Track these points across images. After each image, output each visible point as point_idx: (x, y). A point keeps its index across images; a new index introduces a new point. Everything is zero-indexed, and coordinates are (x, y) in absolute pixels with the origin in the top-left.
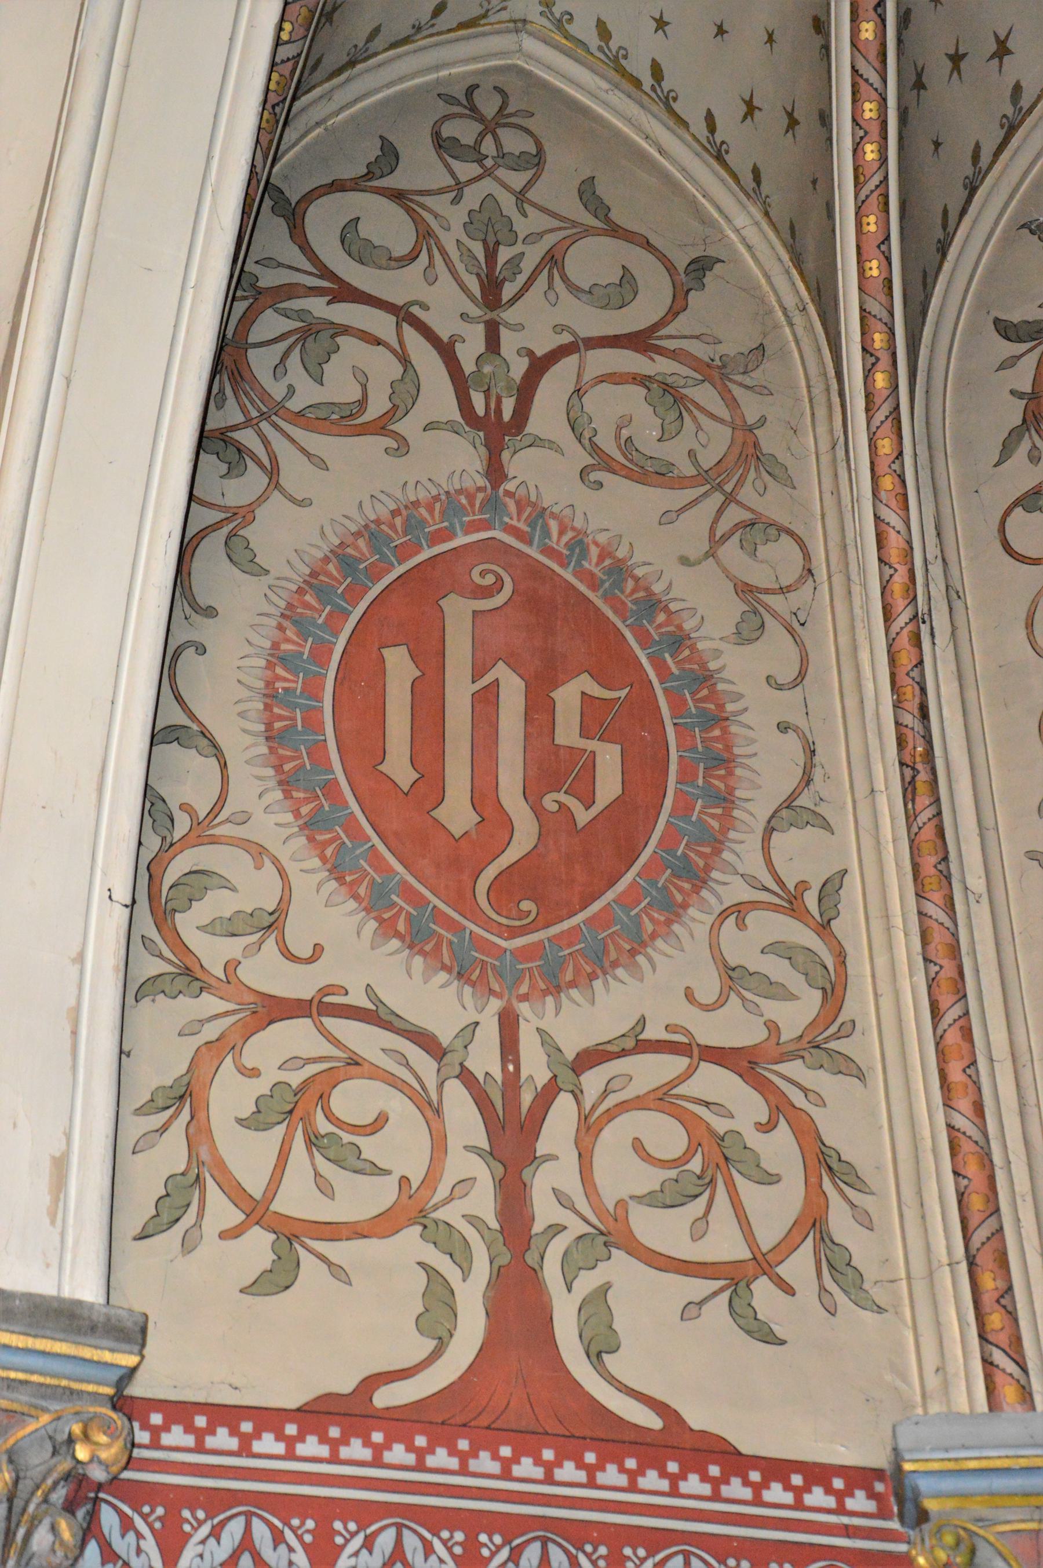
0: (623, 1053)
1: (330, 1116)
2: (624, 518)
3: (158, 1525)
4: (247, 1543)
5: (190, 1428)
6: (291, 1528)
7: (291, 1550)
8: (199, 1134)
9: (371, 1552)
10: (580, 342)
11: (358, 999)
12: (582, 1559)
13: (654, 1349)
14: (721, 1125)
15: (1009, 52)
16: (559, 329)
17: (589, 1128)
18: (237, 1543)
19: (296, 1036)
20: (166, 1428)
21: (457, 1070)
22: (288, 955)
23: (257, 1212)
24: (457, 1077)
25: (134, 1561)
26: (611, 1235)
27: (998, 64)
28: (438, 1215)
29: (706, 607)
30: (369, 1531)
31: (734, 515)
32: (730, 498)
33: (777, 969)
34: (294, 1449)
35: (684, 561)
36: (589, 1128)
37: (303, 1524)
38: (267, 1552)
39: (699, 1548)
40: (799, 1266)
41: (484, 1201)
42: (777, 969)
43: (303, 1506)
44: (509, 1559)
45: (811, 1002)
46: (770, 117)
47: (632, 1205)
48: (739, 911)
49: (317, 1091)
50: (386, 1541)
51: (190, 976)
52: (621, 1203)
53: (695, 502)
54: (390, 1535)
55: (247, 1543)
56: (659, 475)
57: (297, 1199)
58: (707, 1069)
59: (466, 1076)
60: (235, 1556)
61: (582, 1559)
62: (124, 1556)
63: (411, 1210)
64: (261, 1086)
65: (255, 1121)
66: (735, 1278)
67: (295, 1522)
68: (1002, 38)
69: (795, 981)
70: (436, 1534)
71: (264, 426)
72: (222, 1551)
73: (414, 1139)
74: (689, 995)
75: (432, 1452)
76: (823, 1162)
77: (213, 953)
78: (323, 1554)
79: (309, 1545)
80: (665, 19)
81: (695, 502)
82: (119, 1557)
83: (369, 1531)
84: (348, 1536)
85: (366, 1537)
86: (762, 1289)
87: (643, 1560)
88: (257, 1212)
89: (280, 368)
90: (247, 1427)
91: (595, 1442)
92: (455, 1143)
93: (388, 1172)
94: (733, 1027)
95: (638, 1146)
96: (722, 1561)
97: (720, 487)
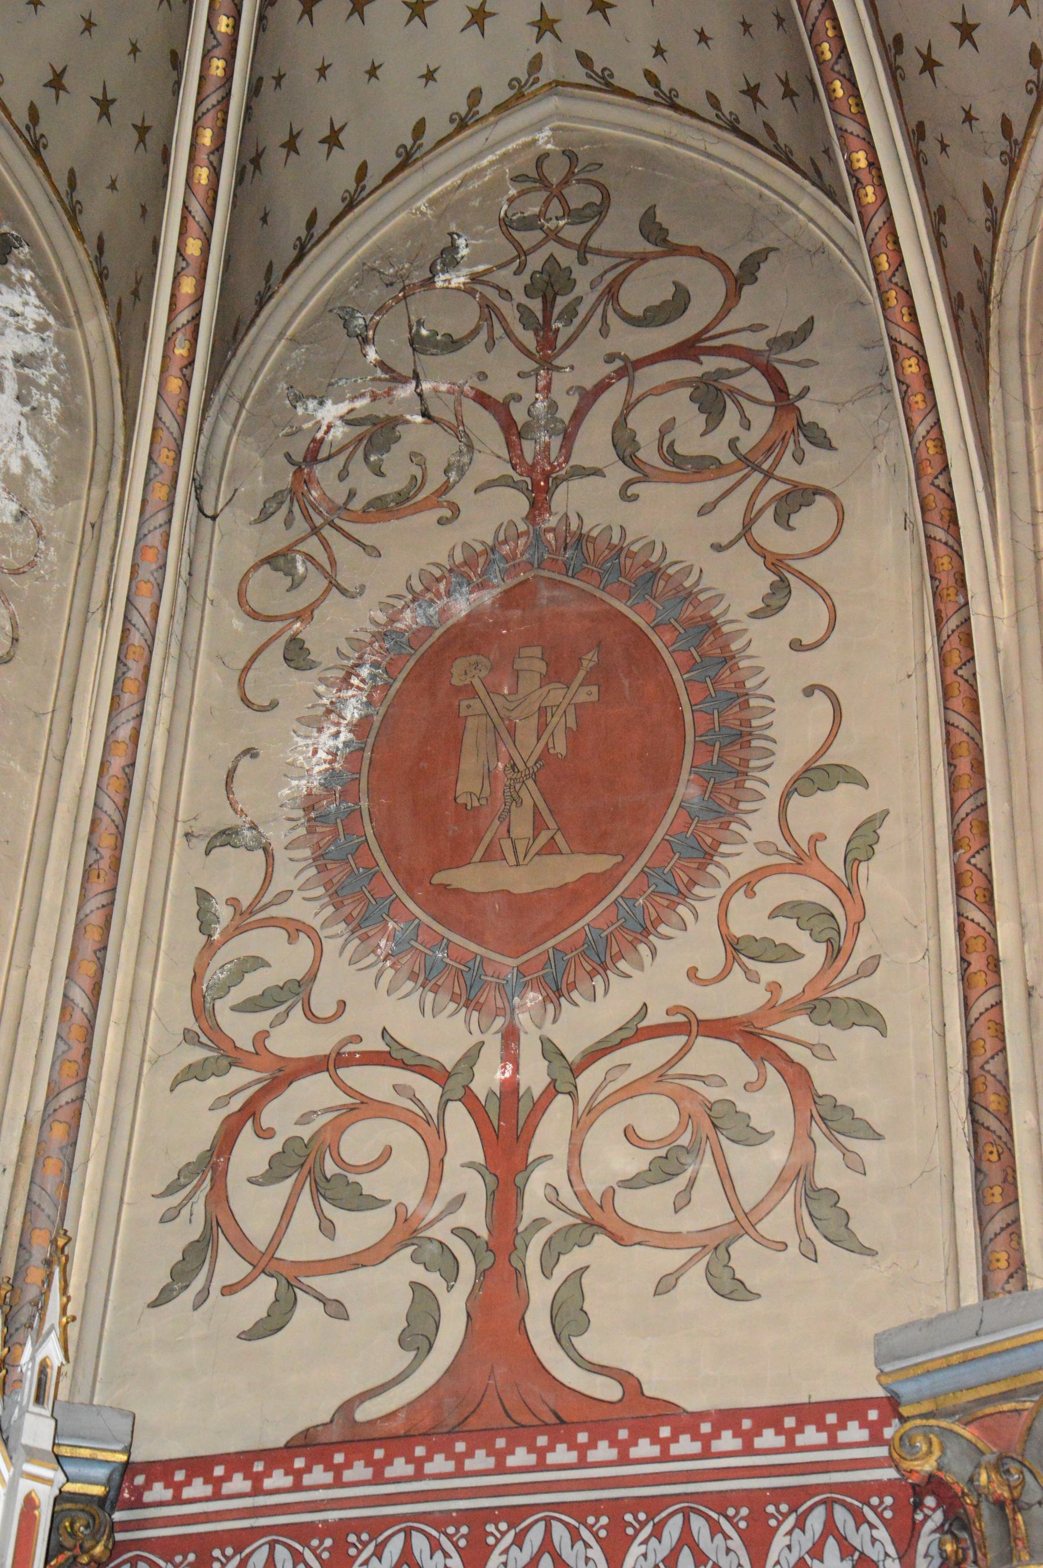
0: (624, 1043)
1: (340, 1161)
2: (667, 521)
3: (603, 1533)
4: (547, 1545)
5: (821, 1427)
6: (727, 1517)
7: (587, 1545)
8: (219, 1195)
9: (803, 1531)
10: (629, 365)
11: (374, 1043)
12: (308, 1555)
13: (643, 1328)
14: (713, 1094)
15: (319, 70)
16: (610, 358)
17: (581, 1126)
18: (535, 1551)
19: (316, 1092)
20: (800, 1429)
21: (460, 1093)
22: (310, 1015)
23: (264, 1262)
24: (460, 1100)
25: (723, 1561)
26: (597, 1221)
27: (552, 37)
28: (428, 1233)
29: (735, 585)
30: (656, 1520)
31: (774, 488)
32: (768, 475)
33: (787, 931)
34: (836, 1437)
35: (718, 548)
36: (581, 1126)
37: (457, 1531)
38: (568, 1554)
39: (291, 1539)
40: (779, 1222)
41: (474, 1216)
42: (787, 931)
43: (595, 1507)
44: (374, 1554)
45: (815, 954)
46: (770, 93)
47: (621, 1193)
48: (748, 884)
49: (327, 1141)
50: (394, 1548)
51: (231, 1056)
52: (610, 1193)
53: (739, 483)
54: (820, 1513)
55: (547, 1545)
56: (703, 467)
57: (302, 1244)
58: (702, 1043)
59: (469, 1099)
60: (674, 1554)
61: (308, 1555)
62: (859, 1548)
63: (407, 1233)
64: (275, 1145)
65: (273, 1174)
66: (716, 1247)
67: (731, 1512)
68: (475, 27)
69: (801, 940)
70: (306, 1544)
71: (327, 532)
72: (805, 1541)
73: (414, 1167)
74: (692, 974)
75: (844, 1427)
76: (821, 1113)
77: (241, 1029)
78: (475, 1555)
79: (462, 1549)
80: (436, 75)
81: (739, 483)
82: (856, 1549)
83: (381, 1539)
84: (499, 1536)
85: (654, 1524)
86: (743, 1250)
87: (229, 1559)
88: (264, 1262)
89: (343, 475)
90: (831, 1418)
91: (543, 1427)
92: (451, 1163)
93: (385, 1203)
94: (738, 997)
95: (629, 1134)
96: (169, 1560)
97: (757, 468)
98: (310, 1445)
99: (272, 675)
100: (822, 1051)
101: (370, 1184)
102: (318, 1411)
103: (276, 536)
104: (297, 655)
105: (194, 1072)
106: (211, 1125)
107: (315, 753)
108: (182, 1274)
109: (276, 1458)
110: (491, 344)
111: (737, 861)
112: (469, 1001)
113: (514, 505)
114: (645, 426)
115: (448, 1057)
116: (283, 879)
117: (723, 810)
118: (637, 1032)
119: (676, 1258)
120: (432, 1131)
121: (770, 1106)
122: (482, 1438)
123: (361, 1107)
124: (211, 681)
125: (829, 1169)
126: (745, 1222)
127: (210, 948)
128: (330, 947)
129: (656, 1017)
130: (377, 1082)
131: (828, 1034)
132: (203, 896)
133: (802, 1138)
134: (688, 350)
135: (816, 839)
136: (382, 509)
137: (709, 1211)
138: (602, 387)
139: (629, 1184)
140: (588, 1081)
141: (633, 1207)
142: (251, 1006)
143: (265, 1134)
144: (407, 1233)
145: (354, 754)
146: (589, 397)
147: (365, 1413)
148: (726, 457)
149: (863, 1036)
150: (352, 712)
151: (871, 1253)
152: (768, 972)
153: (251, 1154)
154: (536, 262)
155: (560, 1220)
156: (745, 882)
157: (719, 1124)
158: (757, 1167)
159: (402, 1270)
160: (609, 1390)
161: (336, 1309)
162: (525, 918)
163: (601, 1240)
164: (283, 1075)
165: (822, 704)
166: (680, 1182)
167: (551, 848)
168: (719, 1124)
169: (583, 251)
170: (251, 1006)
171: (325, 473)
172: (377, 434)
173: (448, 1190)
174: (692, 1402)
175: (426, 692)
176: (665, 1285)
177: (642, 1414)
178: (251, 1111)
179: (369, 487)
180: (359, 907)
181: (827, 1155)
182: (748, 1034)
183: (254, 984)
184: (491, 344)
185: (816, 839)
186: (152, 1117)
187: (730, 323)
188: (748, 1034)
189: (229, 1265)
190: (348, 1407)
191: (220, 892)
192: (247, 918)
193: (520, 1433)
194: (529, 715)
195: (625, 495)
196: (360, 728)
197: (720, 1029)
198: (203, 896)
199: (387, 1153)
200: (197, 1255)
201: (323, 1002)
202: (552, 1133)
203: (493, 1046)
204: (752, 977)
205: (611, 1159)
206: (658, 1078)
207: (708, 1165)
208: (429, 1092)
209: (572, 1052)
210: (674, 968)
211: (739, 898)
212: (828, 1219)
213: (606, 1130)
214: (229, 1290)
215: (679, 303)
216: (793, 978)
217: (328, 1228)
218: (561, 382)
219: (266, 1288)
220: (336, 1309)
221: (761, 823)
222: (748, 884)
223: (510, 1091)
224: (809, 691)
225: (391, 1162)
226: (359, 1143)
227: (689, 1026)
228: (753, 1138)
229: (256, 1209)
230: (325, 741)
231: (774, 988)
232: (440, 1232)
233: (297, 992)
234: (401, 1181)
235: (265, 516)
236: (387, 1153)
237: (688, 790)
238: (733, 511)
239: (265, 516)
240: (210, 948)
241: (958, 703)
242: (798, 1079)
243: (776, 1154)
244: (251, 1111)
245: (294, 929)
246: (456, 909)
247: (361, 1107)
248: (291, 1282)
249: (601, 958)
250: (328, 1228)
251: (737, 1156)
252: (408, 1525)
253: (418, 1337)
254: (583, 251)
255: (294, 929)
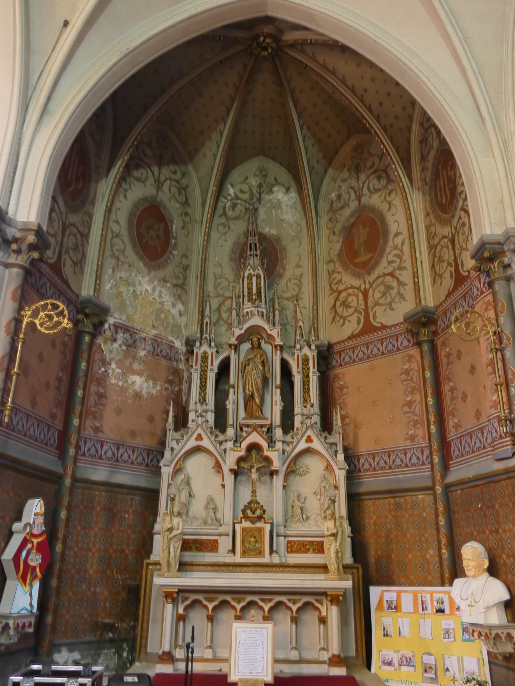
8: (335, 310)
11: (349, 286)
22: (342, 284)
26: (377, 304)
29: (384, 207)
31: (388, 191)
33: (395, 259)
41: (363, 306)
52: (378, 300)
59: (361, 291)
64: (341, 302)
66: (390, 304)
74: (384, 267)
76: (401, 284)
77: (334, 287)
94: (390, 270)
98: (349, 338)
99: (332, 237)
100: (400, 275)
101: (351, 305)
102: (349, 334)
103: (329, 216)
104: (334, 233)
105: (331, 294)
106: (333, 301)
107: (338, 247)
108: (333, 320)
109: (346, 340)
110: (351, 178)
111: (388, 249)
112: (359, 277)
113: (357, 203)
114: (371, 186)
115: (358, 286)
116: (337, 266)
117: (386, 243)
118: (379, 277)
119: (385, 307)
120: (357, 296)
121: (395, 284)
122: (367, 334)
123: (349, 295)
124: (324, 239)
125: (402, 291)
126: (393, 300)
127: (330, 278)
128: (343, 274)
129: (381, 274)
130: (350, 291)
131: (401, 272)
132: (328, 271)
133: (399, 287)
134: (375, 172)
135: (397, 244)
136: (342, 208)
137: (389, 300)
138: (365, 181)
139: (380, 298)
140: (374, 286)
141: (382, 301)
142: (335, 284)
143: (339, 301)
144: (356, 310)
145: (342, 246)
146: (364, 183)
147: (354, 333)
148: (381, 188)
149: (405, 271)
150: (341, 240)
151: (407, 301)
152: (393, 265)
153: (338, 304)
154: (355, 163)
155: (372, 305)
156: (390, 254)
157: (389, 288)
158: (394, 292)
159: (356, 315)
160: (380, 325)
161: (350, 321)
162: (364, 265)
163: (377, 306)
164: (340, 292)
165: (397, 223)
166: (385, 297)
167: (366, 254)
168: (389, 288)
169: (361, 159)
170: (335, 284)
171: (334, 205)
172: (339, 197)
173: (360, 304)
174: (389, 324)
175: (349, 232)
176: (385, 310)
177: (384, 327)
178: (337, 298)
179: (339, 205)
180: (345, 267)
181: (402, 289)
182: (392, 274)
183: (336, 281)
184: (351, 178)
185: (397, 244)
186: (326, 300)
187: (381, 165)
188: (392, 274)
189: (338, 318)
190: (352, 333)
191: (330, 270)
192: (333, 272)
193: (371, 332)
194: (362, 234)
195: (370, 197)
196: (342, 242)
197: (389, 274)
198: (328, 271)
199: (353, 300)
200: (334, 318)
201: (343, 282)
202: (370, 294)
203: (363, 283)
204: (391, 266)
205: (378, 295)
206: (382, 283)
207: (388, 294)
208: (356, 291)
209: (371, 282)
210: (383, 267)
211: (389, 255)
212: (402, 297)
213: (376, 291)
214: (338, 321)
215: (374, 164)
216: (396, 265)
217: (347, 311)
218: (360, 182)
219: (342, 320)
220: (350, 321)
221: (390, 243)
222: (390, 253)
223: (365, 289)
224: (395, 222)
225: (353, 301)
226: (349, 299)
227: (385, 275)
228: (392, 288)
229: (340, 310)
230: (339, 245)
231: (394, 267)
232: (360, 309)
233: (340, 281)
234: (354, 304)
235: (328, 213)
236: (353, 300)
237: (381, 241)
238: (383, 197)
239: (328, 213)
240: (330, 278)
241: (416, 287)
242: (398, 279)
243: (396, 290)
244: (337, 298)
245: (339, 272)
246: (356, 265)
247: (349, 295)
248: (344, 319)
249: (373, 268)
250: (347, 311)
251: (391, 291)
252: (360, 345)
253: (359, 323)
254: (361, 159)
255: (339, 272)
